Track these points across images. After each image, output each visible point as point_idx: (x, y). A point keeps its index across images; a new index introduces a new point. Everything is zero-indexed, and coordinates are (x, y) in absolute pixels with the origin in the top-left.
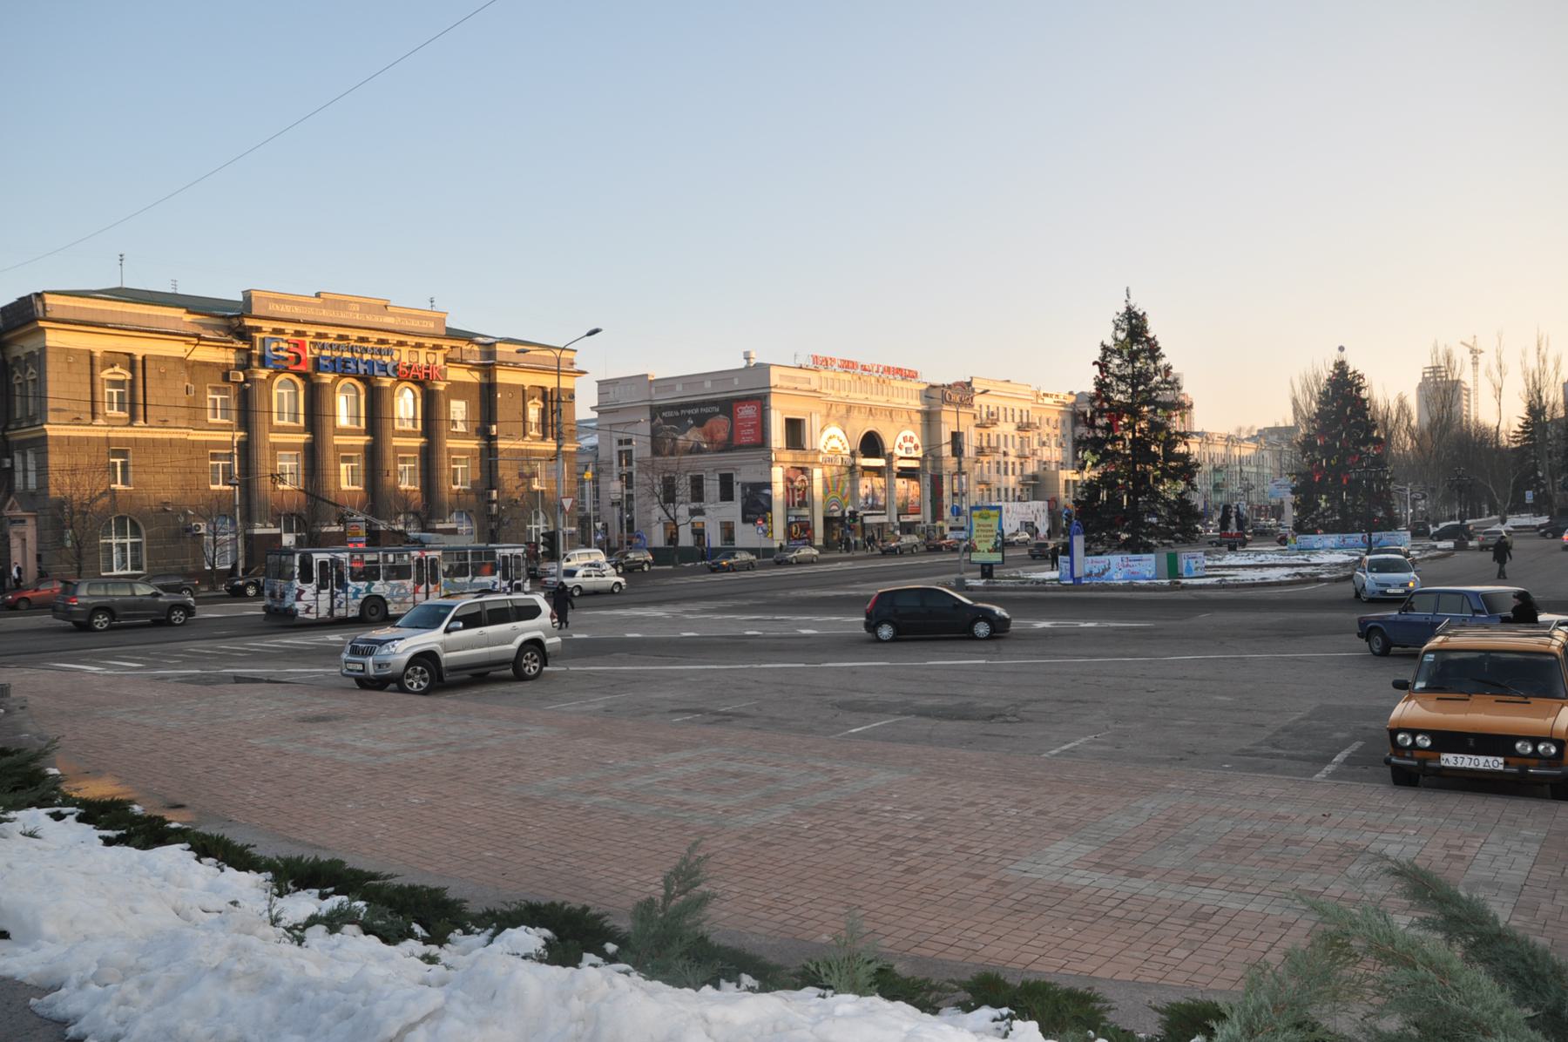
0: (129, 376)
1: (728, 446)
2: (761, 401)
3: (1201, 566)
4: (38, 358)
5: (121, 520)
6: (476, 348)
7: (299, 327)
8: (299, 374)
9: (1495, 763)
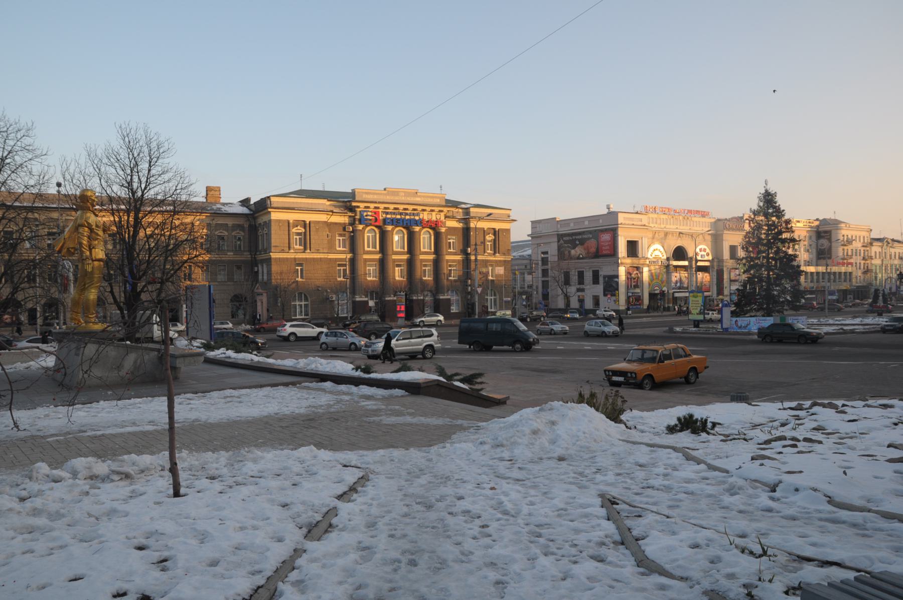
0: (304, 230)
1: (597, 255)
4: (268, 224)
5: (300, 294)
7: (376, 205)
8: (376, 227)
9: (621, 379)
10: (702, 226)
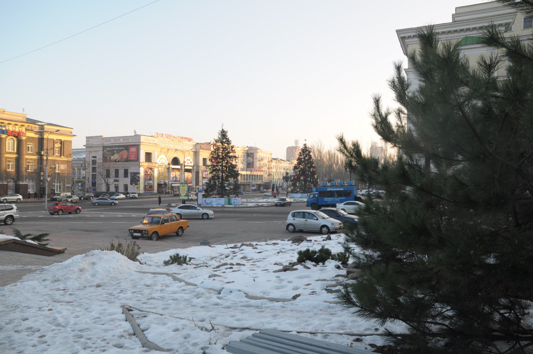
0: (60, 145)
1: (127, 160)
2: (137, 146)
3: (238, 201)
6: (37, 126)
10: (189, 146)
